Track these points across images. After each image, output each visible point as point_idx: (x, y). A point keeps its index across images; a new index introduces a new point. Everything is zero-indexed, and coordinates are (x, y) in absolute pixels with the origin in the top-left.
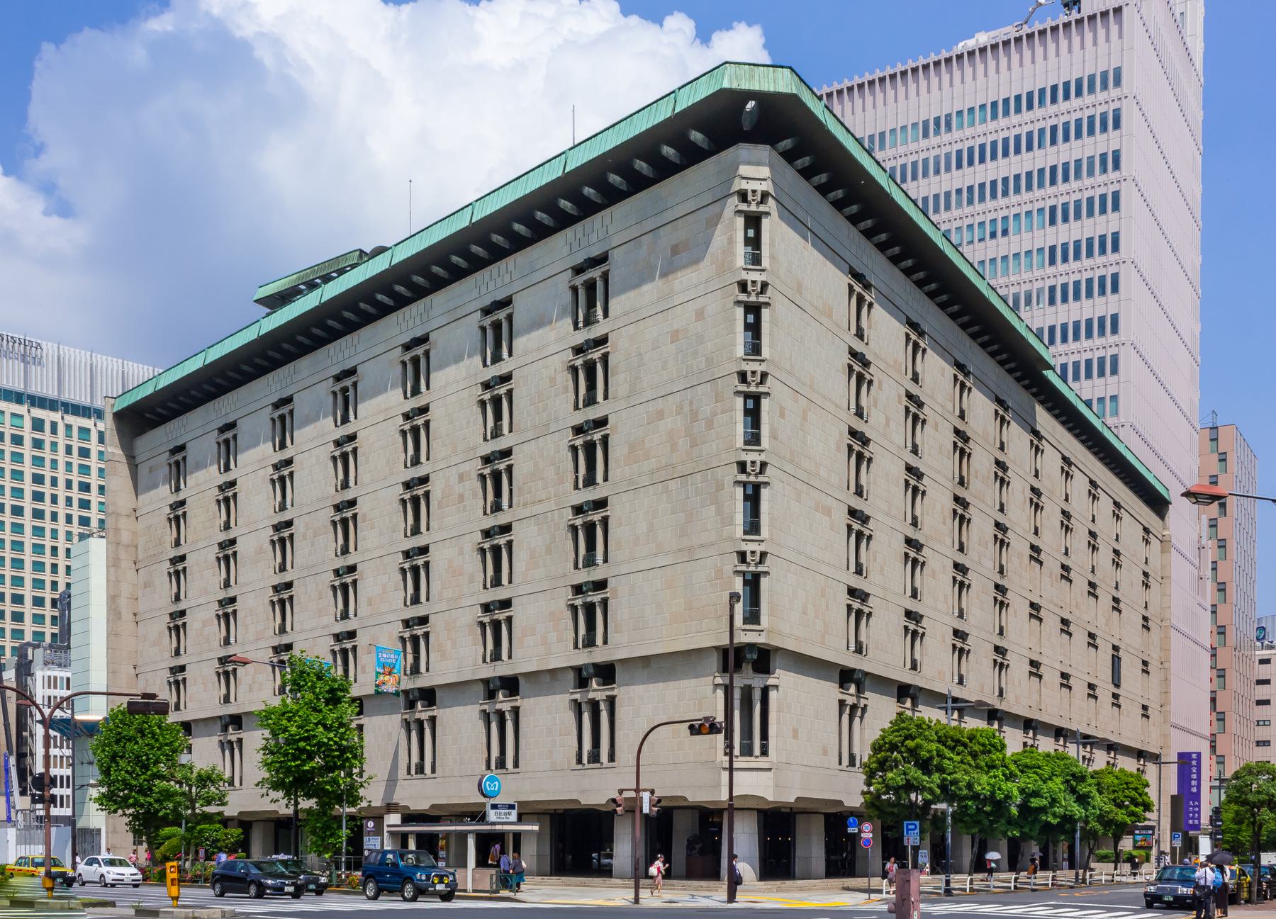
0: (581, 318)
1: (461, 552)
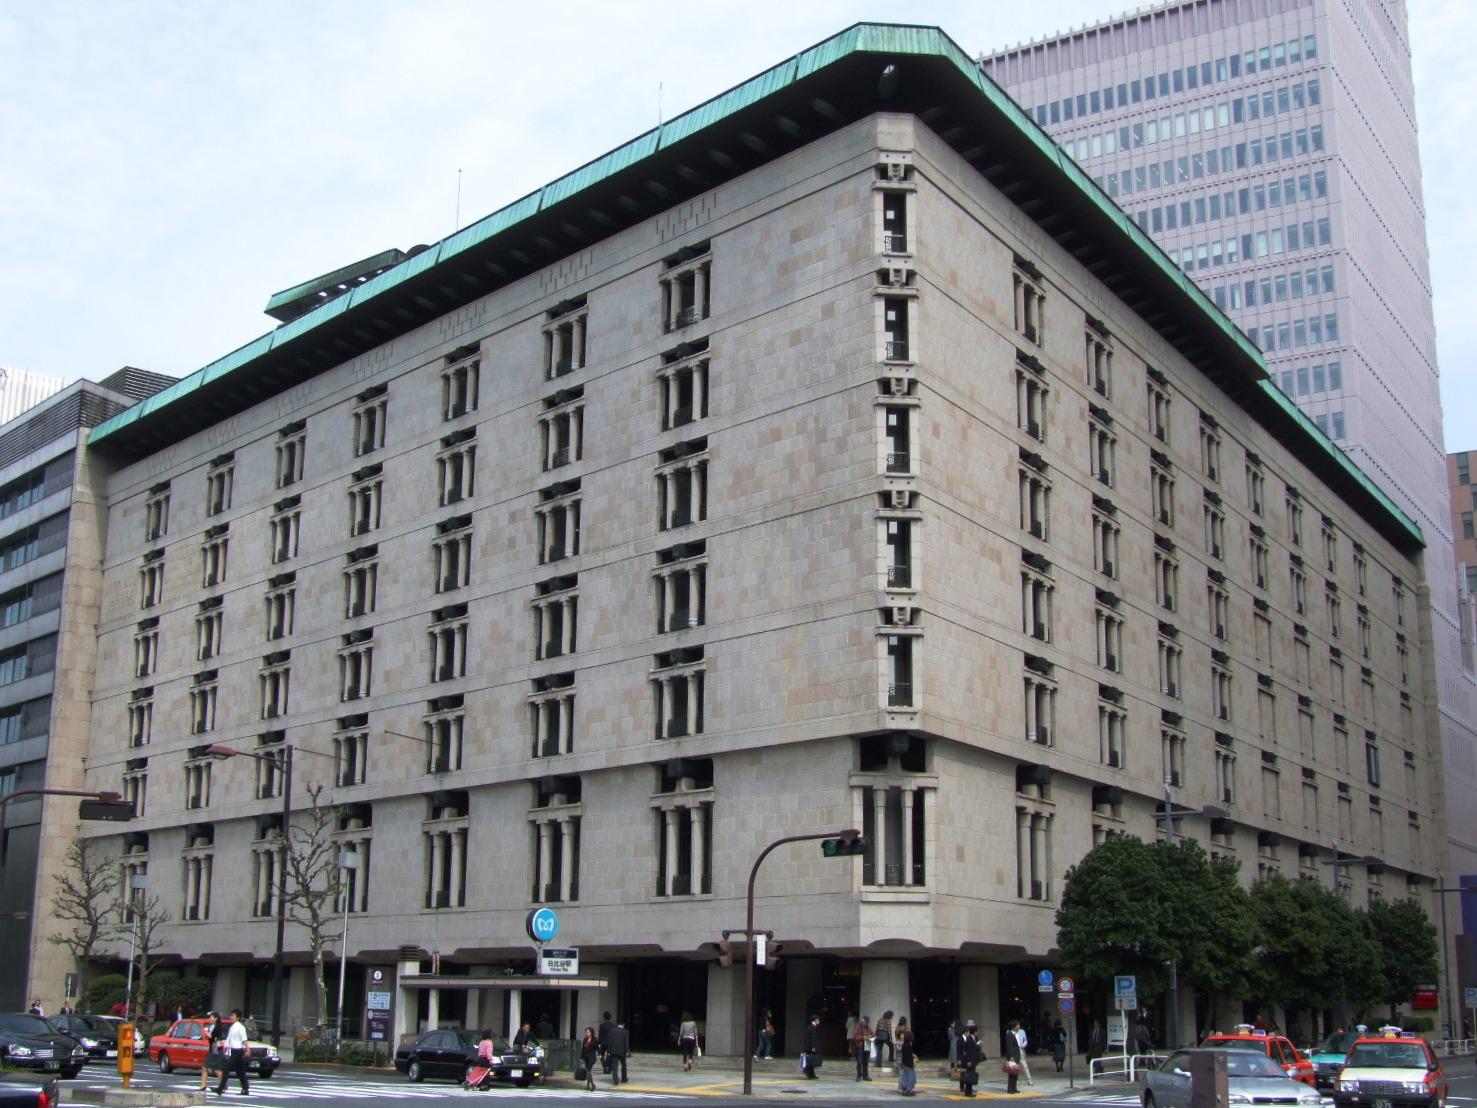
0: (673, 319)
1: (509, 612)
